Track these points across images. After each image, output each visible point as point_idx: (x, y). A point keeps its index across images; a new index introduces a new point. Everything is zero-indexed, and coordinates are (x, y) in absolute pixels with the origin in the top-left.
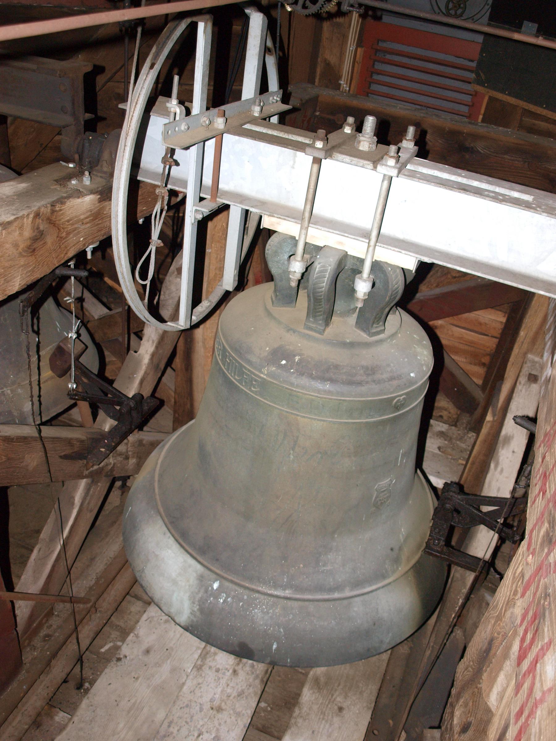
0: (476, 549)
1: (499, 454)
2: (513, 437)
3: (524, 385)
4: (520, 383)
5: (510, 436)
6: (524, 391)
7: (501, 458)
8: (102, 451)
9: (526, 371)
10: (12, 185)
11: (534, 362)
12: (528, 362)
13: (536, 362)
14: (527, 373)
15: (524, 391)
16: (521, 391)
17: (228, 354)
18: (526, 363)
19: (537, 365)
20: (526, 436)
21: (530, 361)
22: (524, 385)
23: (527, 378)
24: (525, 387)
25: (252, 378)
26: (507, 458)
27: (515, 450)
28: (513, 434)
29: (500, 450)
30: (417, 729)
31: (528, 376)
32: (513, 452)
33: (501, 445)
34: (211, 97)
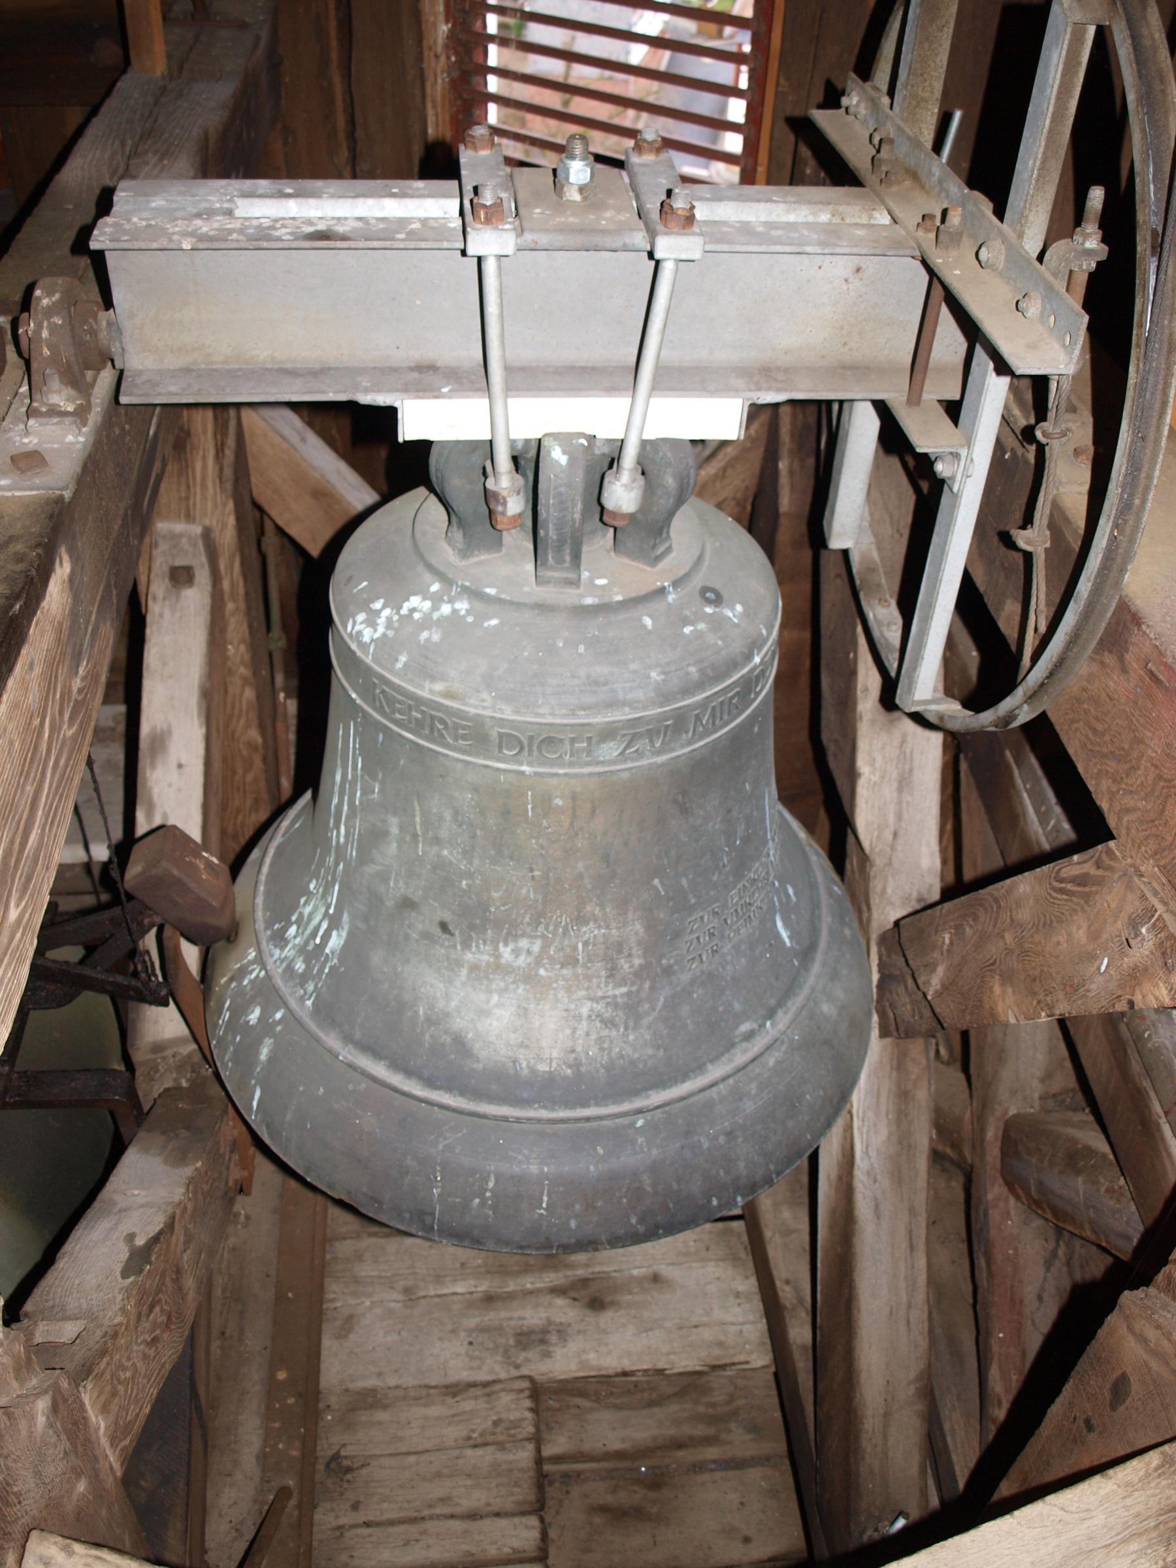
0: (156, 1022)
1: (149, 784)
2: (170, 732)
3: (164, 599)
4: (154, 598)
5: (162, 732)
6: (167, 613)
7: (156, 791)
8: (277, 1010)
9: (161, 564)
10: (160, 394)
11: (174, 537)
12: (160, 541)
13: (181, 535)
14: (166, 568)
15: (167, 613)
16: (161, 615)
17: (375, 680)
18: (156, 545)
19: (184, 541)
20: (199, 717)
21: (164, 537)
22: (164, 599)
23: (167, 580)
24: (167, 603)
25: (432, 717)
26: (170, 785)
27: (183, 762)
28: (170, 725)
29: (148, 774)
30: (143, 1483)
31: (168, 575)
32: (180, 766)
33: (148, 761)
34: (1126, 143)
